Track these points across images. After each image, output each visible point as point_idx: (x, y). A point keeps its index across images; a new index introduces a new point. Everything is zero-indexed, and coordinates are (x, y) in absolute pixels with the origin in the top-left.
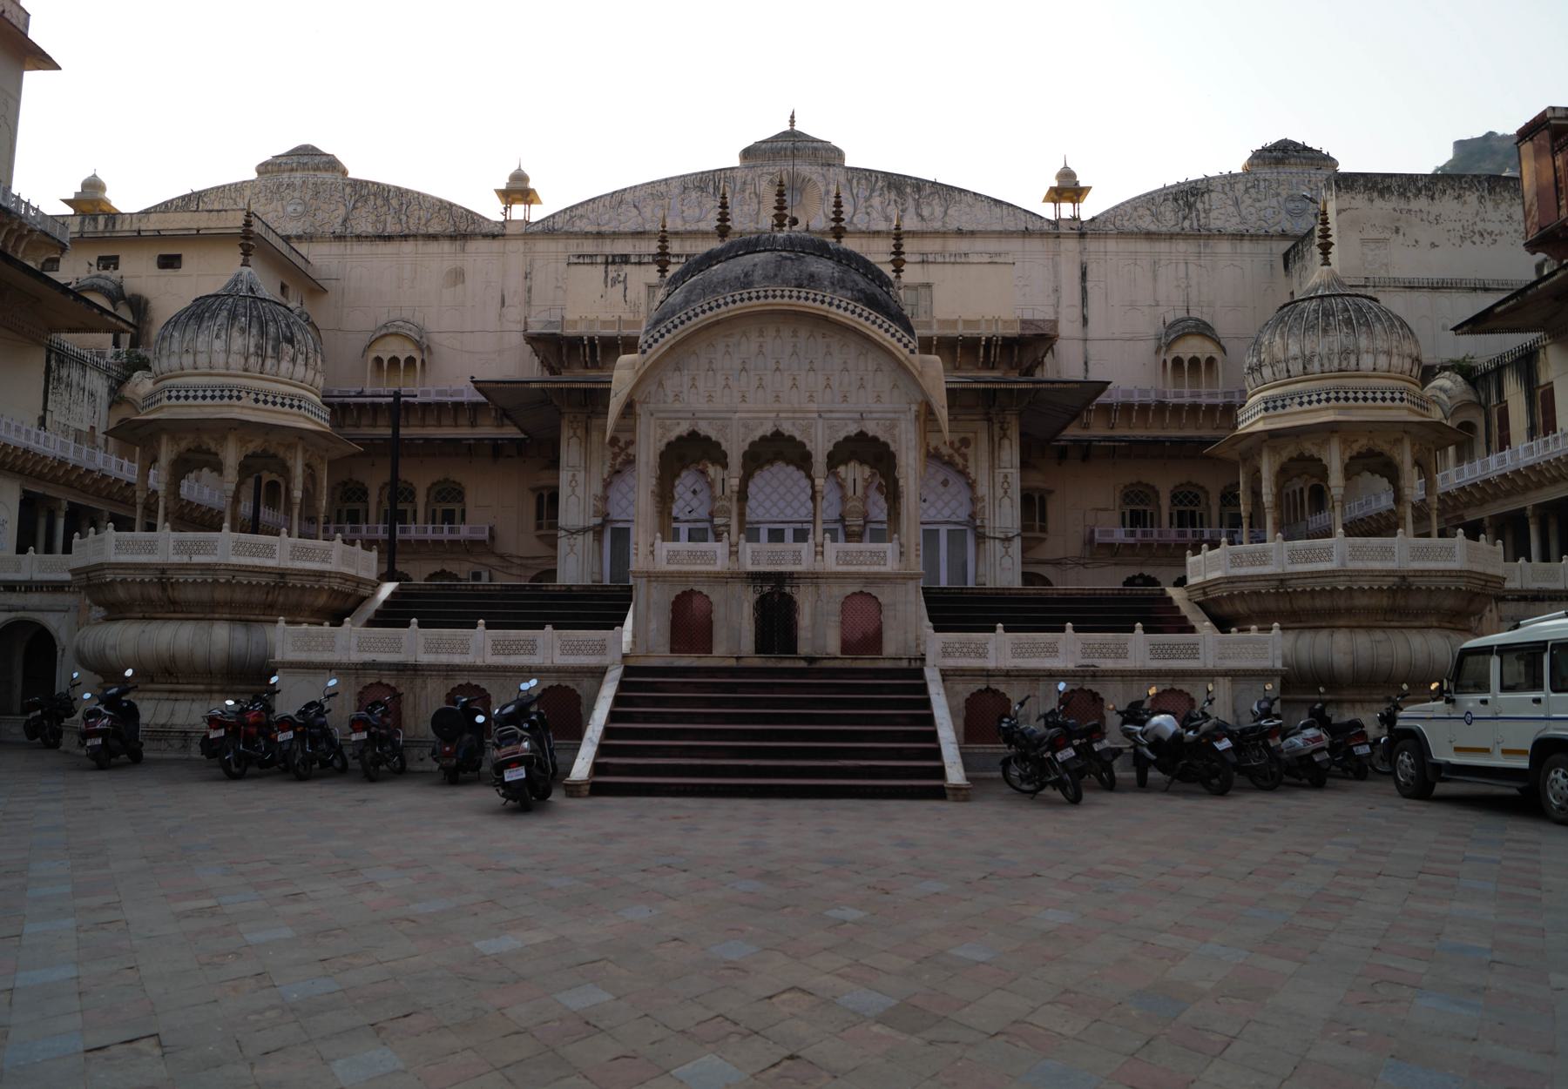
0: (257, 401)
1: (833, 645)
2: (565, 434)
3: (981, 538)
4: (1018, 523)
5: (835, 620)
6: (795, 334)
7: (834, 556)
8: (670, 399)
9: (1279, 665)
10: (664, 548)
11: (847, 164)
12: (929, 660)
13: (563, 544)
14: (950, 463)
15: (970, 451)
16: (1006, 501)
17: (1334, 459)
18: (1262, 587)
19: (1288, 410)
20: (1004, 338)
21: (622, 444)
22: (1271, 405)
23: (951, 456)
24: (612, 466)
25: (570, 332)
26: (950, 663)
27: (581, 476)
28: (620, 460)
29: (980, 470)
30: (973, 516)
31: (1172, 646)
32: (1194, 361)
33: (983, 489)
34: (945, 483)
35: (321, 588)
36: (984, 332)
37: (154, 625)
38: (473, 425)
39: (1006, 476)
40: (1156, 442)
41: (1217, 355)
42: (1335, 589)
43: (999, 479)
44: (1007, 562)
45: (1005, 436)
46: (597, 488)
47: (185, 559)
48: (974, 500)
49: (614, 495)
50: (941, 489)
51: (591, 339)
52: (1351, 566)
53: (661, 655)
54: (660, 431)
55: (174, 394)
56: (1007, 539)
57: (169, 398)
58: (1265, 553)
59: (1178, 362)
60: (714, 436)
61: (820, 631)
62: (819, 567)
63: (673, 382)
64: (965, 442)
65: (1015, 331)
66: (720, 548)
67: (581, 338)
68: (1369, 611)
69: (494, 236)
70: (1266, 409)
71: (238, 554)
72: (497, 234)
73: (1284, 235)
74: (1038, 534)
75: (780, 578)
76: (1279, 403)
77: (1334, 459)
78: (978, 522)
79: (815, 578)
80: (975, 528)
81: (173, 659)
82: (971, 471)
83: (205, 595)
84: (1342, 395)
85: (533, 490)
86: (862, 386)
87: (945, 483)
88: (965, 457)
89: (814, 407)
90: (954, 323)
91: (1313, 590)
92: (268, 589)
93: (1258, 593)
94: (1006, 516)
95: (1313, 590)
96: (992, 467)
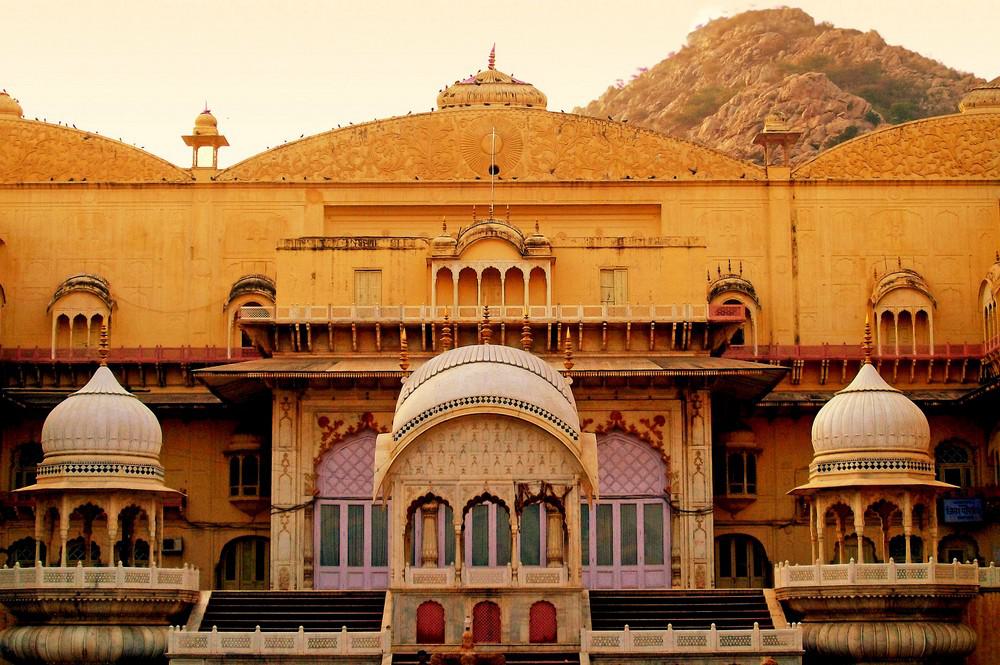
0: (127, 471)
1: (525, 634)
2: (277, 413)
3: (675, 511)
4: (710, 496)
6: (497, 427)
7: (525, 576)
8: (415, 471)
9: (801, 649)
10: (412, 572)
11: (550, 108)
12: (583, 647)
13: (276, 521)
14: (646, 440)
15: (664, 429)
16: (699, 477)
17: (858, 508)
19: (831, 472)
20: (694, 324)
21: (331, 424)
22: (822, 467)
23: (646, 434)
24: (323, 446)
26: (596, 650)
27: (292, 456)
28: (329, 440)
29: (674, 448)
30: (667, 491)
31: (733, 638)
32: (905, 316)
33: (676, 466)
35: (176, 601)
37: (69, 630)
38: (162, 384)
39: (699, 453)
41: (929, 310)
43: (692, 456)
44: (700, 535)
46: (308, 468)
48: (668, 476)
49: (324, 473)
51: (303, 326)
53: (412, 646)
54: (407, 493)
55: (71, 467)
56: (699, 513)
57: (68, 470)
58: (810, 572)
59: (888, 316)
61: (516, 628)
62: (514, 584)
63: (416, 459)
64: (660, 420)
66: (448, 571)
67: (294, 326)
68: (878, 610)
69: (180, 185)
70: (819, 470)
71: (127, 581)
72: (185, 182)
74: (747, 496)
76: (827, 467)
77: (858, 508)
78: (673, 497)
80: (670, 503)
82: (666, 447)
83: (105, 608)
84: (863, 464)
85: (227, 454)
86: (542, 462)
88: (659, 434)
89: (509, 476)
91: (837, 598)
94: (699, 489)
95: (837, 598)
96: (685, 443)
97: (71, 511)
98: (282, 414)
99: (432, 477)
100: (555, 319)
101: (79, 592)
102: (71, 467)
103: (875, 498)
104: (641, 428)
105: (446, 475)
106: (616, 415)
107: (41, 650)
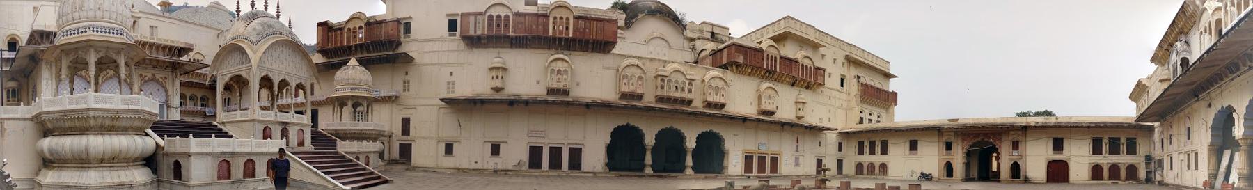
3: (169, 107)
25: (48, 30)
29: (169, 87)
75: (286, 123)
92: (112, 119)
101: (117, 111)
107: (92, 151)
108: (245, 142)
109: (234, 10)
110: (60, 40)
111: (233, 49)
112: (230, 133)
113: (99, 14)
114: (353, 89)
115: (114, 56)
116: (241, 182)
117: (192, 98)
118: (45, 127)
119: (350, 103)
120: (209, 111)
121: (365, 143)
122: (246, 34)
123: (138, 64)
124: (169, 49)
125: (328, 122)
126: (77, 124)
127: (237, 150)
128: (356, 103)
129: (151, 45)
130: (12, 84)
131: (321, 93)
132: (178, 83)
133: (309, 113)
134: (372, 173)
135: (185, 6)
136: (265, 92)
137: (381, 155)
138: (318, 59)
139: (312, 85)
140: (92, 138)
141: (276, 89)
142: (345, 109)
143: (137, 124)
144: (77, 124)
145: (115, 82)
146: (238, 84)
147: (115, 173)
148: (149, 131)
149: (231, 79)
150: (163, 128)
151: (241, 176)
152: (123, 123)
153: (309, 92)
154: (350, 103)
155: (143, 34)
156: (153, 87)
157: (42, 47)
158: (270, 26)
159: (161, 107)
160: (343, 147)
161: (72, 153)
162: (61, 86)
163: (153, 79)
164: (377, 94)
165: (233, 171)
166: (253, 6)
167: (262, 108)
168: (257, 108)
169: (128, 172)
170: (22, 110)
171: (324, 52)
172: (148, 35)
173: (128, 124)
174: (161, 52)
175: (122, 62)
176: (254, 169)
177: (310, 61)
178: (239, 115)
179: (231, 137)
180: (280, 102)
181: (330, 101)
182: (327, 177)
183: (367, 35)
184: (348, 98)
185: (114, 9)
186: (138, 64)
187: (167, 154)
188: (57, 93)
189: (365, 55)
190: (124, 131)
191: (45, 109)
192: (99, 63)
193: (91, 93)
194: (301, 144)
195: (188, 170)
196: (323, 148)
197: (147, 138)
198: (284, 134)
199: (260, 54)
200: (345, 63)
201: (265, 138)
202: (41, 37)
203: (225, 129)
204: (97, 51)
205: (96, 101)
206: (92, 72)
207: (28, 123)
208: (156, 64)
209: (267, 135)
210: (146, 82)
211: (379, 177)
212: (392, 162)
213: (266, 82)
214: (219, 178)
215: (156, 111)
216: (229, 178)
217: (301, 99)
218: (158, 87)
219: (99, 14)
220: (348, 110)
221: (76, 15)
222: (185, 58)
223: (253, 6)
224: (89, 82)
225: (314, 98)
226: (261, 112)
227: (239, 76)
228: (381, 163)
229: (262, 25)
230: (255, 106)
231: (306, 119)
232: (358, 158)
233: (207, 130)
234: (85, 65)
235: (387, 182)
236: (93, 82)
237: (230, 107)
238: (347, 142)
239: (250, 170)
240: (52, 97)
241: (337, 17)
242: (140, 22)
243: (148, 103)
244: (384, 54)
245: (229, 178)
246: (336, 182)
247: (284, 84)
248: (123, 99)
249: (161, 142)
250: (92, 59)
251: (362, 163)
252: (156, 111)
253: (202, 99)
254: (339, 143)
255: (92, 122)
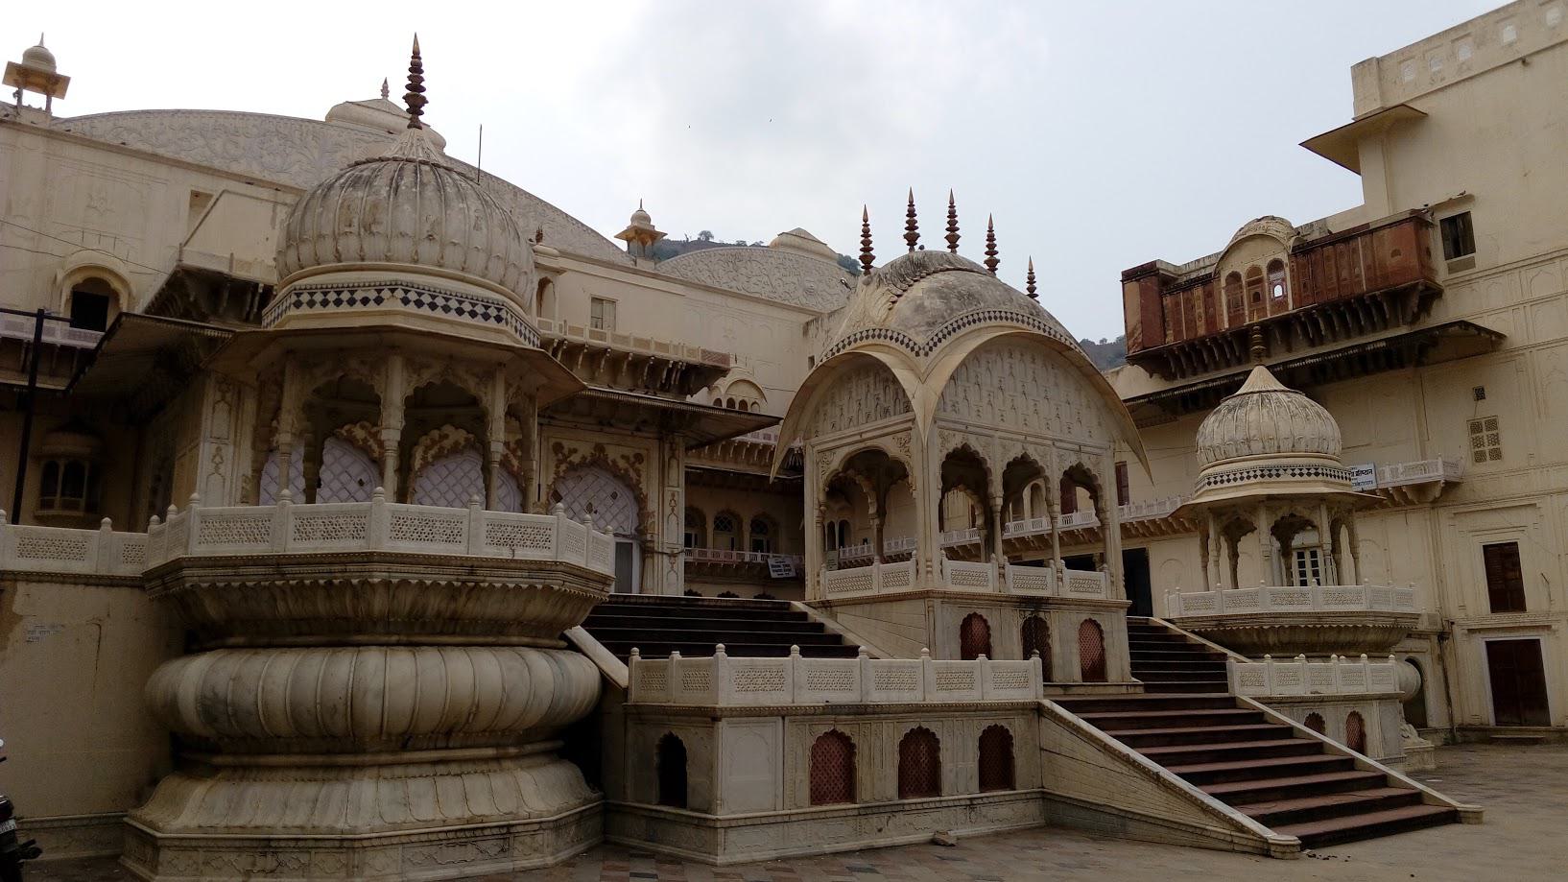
3: (647, 552)
5: (1075, 648)
16: (673, 518)
18: (1301, 623)
25: (240, 273)
29: (651, 489)
33: (653, 506)
34: (614, 496)
36: (672, 356)
40: (740, 476)
42: (1365, 627)
43: (668, 497)
45: (673, 456)
47: (505, 554)
50: (610, 501)
52: (1377, 608)
56: (673, 555)
60: (982, 453)
64: (639, 458)
65: (696, 359)
73: (801, 310)
75: (1037, 603)
79: (1062, 603)
81: (476, 709)
87: (614, 496)
88: (638, 472)
89: (1050, 434)
90: (646, 343)
92: (452, 592)
93: (1297, 627)
96: (662, 484)
97: (410, 392)
98: (218, 396)
99: (972, 419)
100: (562, 335)
101: (472, 566)
102: (413, 296)
103: (1285, 511)
104: (622, 464)
105: (987, 420)
106: (600, 448)
107: (371, 705)
108: (896, 671)
109: (856, 254)
110: (286, 317)
111: (854, 371)
112: (851, 638)
113: (429, 251)
114: (1267, 473)
115: (471, 385)
116: (893, 810)
117: (724, 523)
118: (192, 611)
119: (1264, 522)
120: (777, 564)
121: (1338, 663)
122: (893, 324)
123: (549, 415)
124: (650, 370)
125: (1185, 591)
126: (330, 606)
127: (877, 697)
128: (1288, 520)
129: (595, 356)
130: (69, 445)
131: (1156, 491)
132: (677, 477)
133: (1116, 564)
134: (1382, 781)
135: (705, 242)
136: (960, 502)
137: (1414, 709)
138: (1132, 383)
139: (1120, 471)
140: (373, 661)
141: (997, 489)
142: (1246, 544)
143: (538, 609)
144: (322, 607)
145: (468, 468)
146: (872, 479)
147: (450, 786)
148: (579, 634)
149: (851, 462)
150: (628, 624)
151: (891, 787)
152: (492, 608)
153: (1110, 492)
154: (1264, 522)
155: (569, 318)
156: (599, 486)
157: (212, 328)
158: (971, 297)
159: (623, 551)
160: (1254, 681)
161: (294, 712)
162: (272, 469)
163: (598, 461)
164: (1366, 483)
165: (863, 772)
166: (912, 238)
167: (953, 553)
168: (937, 555)
169: (498, 781)
170: (102, 548)
171: (1150, 359)
172: (586, 324)
173: (511, 609)
174: (624, 377)
175: (497, 404)
176: (935, 765)
177: (1106, 392)
178: (878, 579)
179: (852, 652)
180: (1014, 530)
181: (1189, 521)
182: (1200, 793)
183: (1300, 290)
184: (1254, 504)
185: (479, 239)
186: (549, 415)
187: (642, 715)
188: (253, 492)
189: (1304, 353)
190: (494, 633)
191: (199, 550)
192: (415, 404)
193: (384, 502)
194: (1095, 671)
195: (710, 769)
196: (1175, 687)
197: (570, 660)
198: (1035, 639)
199: (939, 381)
200: (1232, 386)
201: (968, 653)
202: (197, 291)
203: (832, 626)
204: (413, 365)
205: (399, 527)
206: (391, 433)
207: (122, 597)
208: (607, 415)
209: (974, 642)
210: (571, 469)
211: (1417, 798)
212: (1463, 737)
213: (963, 469)
214: (817, 798)
215: (604, 565)
216: (849, 794)
217: (1084, 517)
218: (613, 486)
219: (429, 251)
220: (1258, 546)
221: (350, 245)
222: (701, 398)
223: (912, 238)
224: (378, 463)
225: (1129, 514)
226: (951, 565)
227: (877, 454)
228: (1414, 739)
229: (942, 293)
230: (930, 549)
231: (1105, 585)
232: (1316, 722)
233: (775, 628)
234: (370, 408)
235: (1452, 817)
236: (391, 463)
237: (852, 551)
238: (1268, 662)
239: (920, 771)
240: (228, 505)
241: (1187, 244)
242: (561, 283)
243: (578, 540)
244: (1376, 339)
245: (849, 794)
246: (1239, 816)
247: (1023, 471)
248: (495, 526)
249: (619, 672)
250: (396, 389)
251: (1336, 741)
252: (604, 565)
253: (758, 526)
254: (1238, 666)
255: (379, 604)
